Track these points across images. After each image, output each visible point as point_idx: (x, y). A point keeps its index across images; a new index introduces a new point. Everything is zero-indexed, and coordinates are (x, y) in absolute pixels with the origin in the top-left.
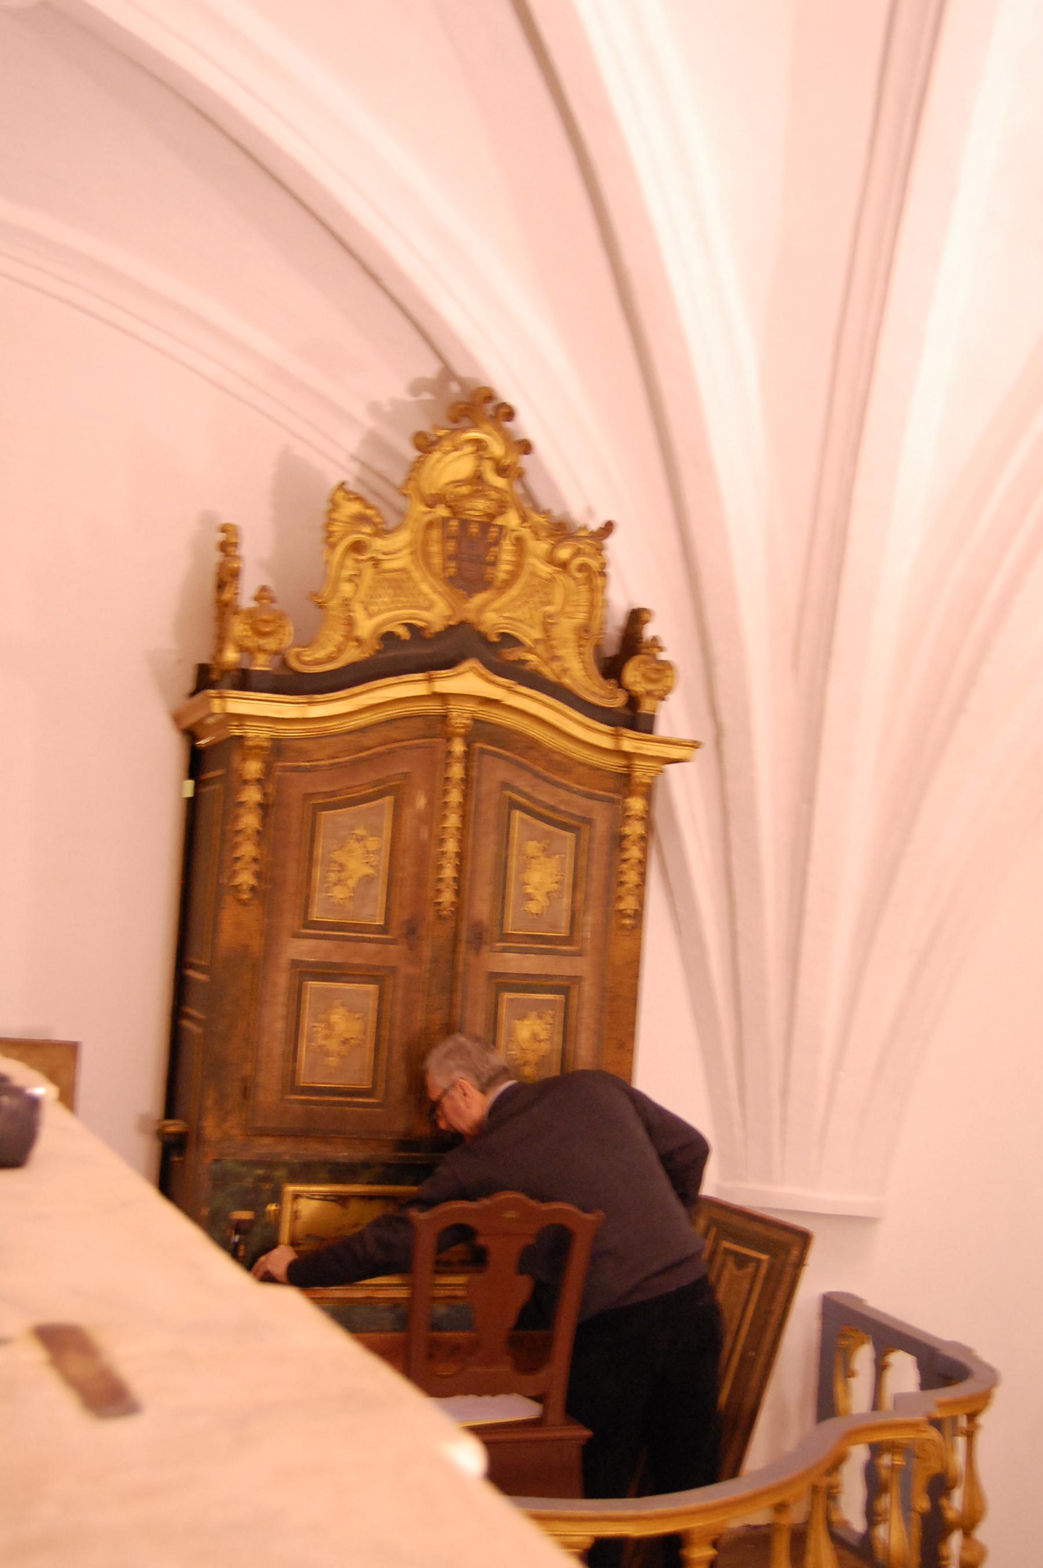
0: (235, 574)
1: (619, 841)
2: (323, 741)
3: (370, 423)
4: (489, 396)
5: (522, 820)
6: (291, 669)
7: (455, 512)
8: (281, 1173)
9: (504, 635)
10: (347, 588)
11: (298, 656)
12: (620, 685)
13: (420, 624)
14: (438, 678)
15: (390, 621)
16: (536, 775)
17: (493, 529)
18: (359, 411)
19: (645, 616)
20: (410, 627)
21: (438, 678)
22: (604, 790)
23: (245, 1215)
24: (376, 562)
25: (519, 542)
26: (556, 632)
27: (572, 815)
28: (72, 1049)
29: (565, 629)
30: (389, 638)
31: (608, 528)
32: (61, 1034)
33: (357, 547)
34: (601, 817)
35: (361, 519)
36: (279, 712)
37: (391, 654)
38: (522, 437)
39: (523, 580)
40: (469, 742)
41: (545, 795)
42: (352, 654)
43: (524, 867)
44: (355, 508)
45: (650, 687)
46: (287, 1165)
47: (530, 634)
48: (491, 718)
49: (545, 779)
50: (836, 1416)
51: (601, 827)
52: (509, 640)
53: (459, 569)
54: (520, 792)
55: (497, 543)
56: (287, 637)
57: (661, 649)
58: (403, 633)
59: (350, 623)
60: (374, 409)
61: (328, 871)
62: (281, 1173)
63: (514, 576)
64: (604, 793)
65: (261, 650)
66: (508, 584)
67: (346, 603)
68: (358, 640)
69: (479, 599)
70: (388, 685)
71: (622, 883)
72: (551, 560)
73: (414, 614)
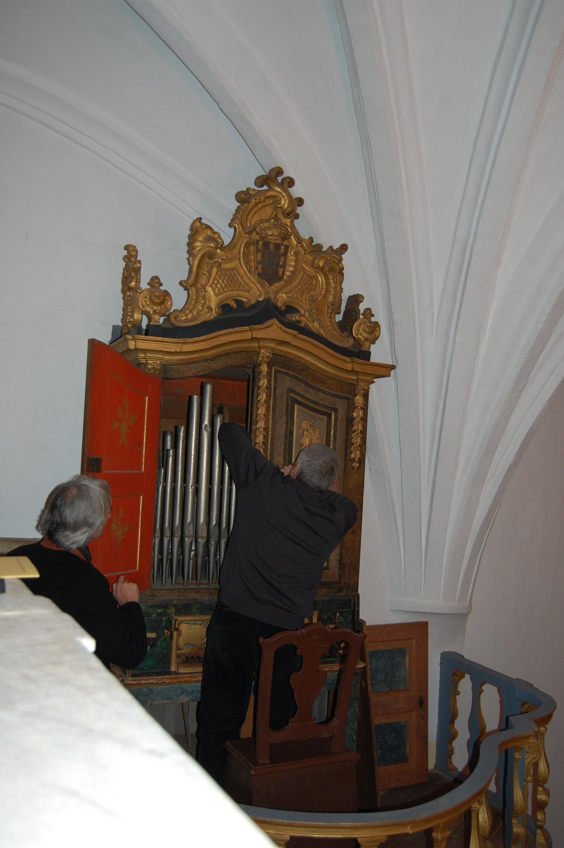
1: (350, 421)
5: (299, 409)
6: (173, 324)
11: (176, 318)
16: (306, 384)
22: (342, 392)
27: (326, 407)
31: (344, 248)
32: (174, 427)
34: (341, 406)
36: (166, 348)
40: (270, 366)
41: (312, 395)
46: (175, 606)
48: (191, 569)
51: (342, 414)
53: (263, 268)
54: (300, 395)
55: (285, 254)
57: (373, 316)
62: (172, 611)
70: (242, 331)
71: (352, 444)
72: (312, 265)
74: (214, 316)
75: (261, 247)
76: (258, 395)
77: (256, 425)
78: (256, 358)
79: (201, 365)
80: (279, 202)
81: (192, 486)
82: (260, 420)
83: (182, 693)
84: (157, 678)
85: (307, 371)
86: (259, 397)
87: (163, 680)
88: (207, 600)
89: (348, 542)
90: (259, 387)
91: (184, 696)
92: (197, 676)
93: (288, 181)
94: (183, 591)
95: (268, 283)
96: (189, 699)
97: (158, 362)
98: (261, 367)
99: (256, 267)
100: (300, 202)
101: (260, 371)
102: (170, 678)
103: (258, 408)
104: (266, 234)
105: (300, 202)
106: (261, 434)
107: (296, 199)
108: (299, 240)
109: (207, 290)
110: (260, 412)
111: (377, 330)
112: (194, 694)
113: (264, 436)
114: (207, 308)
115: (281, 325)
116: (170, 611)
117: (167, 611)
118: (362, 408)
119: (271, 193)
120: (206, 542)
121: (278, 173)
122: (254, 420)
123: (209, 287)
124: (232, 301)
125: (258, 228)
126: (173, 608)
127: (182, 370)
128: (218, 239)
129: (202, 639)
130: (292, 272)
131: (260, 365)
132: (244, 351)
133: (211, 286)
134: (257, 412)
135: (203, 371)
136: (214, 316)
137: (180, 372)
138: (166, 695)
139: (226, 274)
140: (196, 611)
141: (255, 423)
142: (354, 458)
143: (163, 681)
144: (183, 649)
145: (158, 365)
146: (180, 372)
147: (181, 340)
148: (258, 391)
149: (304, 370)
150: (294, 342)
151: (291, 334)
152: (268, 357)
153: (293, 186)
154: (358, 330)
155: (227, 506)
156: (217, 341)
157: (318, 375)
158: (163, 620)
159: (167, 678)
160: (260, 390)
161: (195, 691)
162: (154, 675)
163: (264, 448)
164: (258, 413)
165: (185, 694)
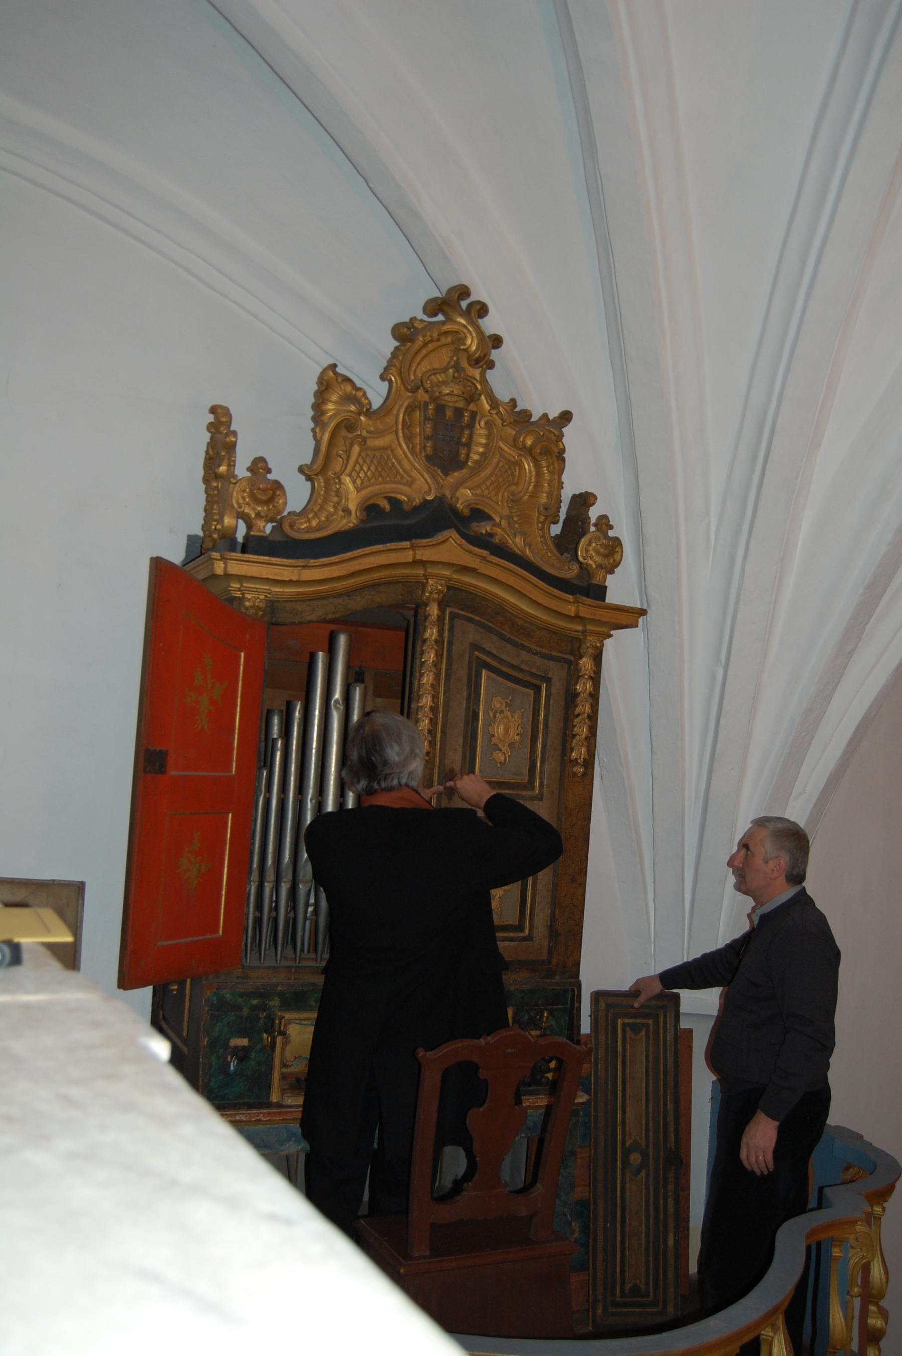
0: (231, 448)
1: (571, 698)
4: (463, 291)
5: (488, 677)
6: (286, 536)
14: (420, 546)
16: (501, 637)
19: (592, 499)
21: (420, 546)
22: (560, 652)
23: (244, 1042)
25: (489, 425)
28: (80, 887)
31: (566, 417)
37: (377, 524)
38: (492, 332)
41: (509, 654)
43: (489, 722)
46: (281, 995)
49: (510, 641)
50: (885, 1334)
51: (558, 686)
52: (478, 515)
53: (435, 448)
55: (471, 426)
57: (611, 528)
58: (385, 505)
61: (401, 785)
62: (275, 1002)
64: (559, 654)
67: (211, 461)
71: (574, 736)
72: (514, 444)
79: (331, 603)
86: (424, 656)
91: (291, 1143)
93: (478, 307)
94: (293, 970)
96: (300, 1147)
100: (497, 341)
103: (422, 675)
105: (497, 341)
109: (343, 481)
111: (618, 551)
114: (343, 511)
116: (271, 1003)
119: (450, 326)
122: (416, 695)
132: (401, 582)
133: (350, 475)
134: (420, 680)
135: (334, 613)
137: (296, 613)
140: (314, 1004)
143: (258, 1118)
145: (261, 601)
147: (300, 562)
148: (422, 646)
152: (440, 592)
158: (260, 1018)
165: (293, 1139)
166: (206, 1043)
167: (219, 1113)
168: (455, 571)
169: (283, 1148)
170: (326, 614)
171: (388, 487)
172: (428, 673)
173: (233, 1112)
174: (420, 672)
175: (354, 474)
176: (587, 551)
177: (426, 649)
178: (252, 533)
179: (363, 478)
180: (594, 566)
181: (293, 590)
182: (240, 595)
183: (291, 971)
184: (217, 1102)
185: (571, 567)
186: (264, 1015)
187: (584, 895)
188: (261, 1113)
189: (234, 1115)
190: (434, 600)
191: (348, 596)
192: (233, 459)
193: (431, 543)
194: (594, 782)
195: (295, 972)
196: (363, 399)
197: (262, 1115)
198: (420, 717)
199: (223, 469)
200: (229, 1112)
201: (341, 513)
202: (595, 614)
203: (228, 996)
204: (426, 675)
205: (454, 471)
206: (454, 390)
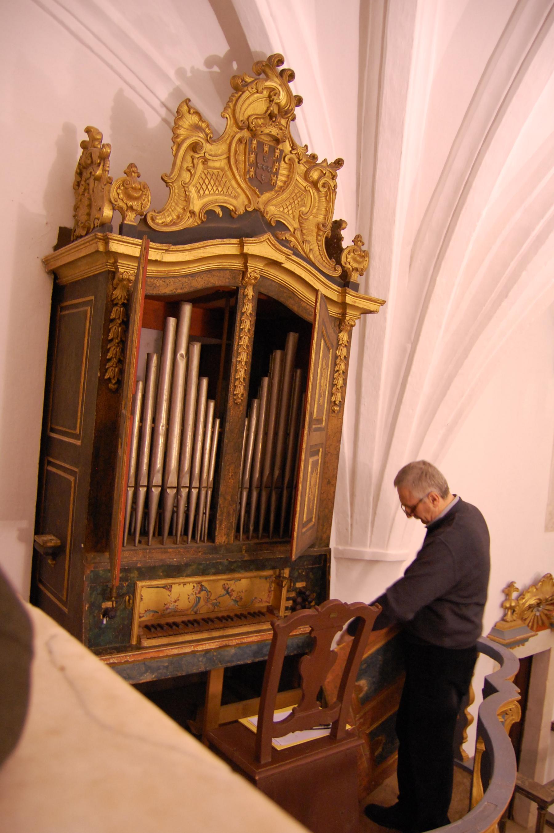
2: (168, 280)
3: (177, 83)
7: (254, 134)
8: (135, 574)
9: (278, 222)
10: (186, 176)
11: (153, 219)
12: (339, 262)
13: (231, 208)
15: (212, 202)
17: (278, 151)
18: (171, 73)
19: (343, 226)
20: (222, 207)
24: (205, 161)
26: (306, 225)
29: (311, 225)
30: (210, 213)
31: (339, 163)
33: (195, 147)
35: (197, 128)
37: (212, 225)
39: (291, 188)
42: (188, 222)
44: (195, 119)
45: (355, 265)
46: (139, 569)
47: (292, 224)
56: (148, 203)
59: (187, 199)
60: (180, 72)
62: (135, 574)
63: (286, 184)
65: (131, 208)
66: (282, 189)
68: (193, 213)
69: (266, 196)
72: (306, 177)
73: (228, 200)
74: (198, 223)
75: (255, 147)
76: (241, 322)
77: (237, 358)
78: (241, 279)
79: (180, 281)
80: (277, 94)
81: (162, 426)
82: (243, 351)
83: (146, 671)
84: (119, 655)
85: (294, 300)
86: (242, 325)
87: (126, 658)
88: (175, 561)
89: (324, 492)
90: (243, 314)
91: (148, 674)
92: (165, 650)
93: (289, 73)
94: (148, 551)
95: (259, 191)
96: (154, 676)
97: (132, 272)
98: (246, 290)
99: (247, 170)
100: (299, 101)
101: (245, 294)
102: (133, 655)
103: (240, 338)
104: (262, 132)
105: (299, 101)
106: (242, 368)
107: (296, 96)
108: (294, 147)
109: (190, 189)
110: (242, 343)
111: (366, 261)
112: (160, 671)
113: (343, 379)
114: (190, 212)
115: (276, 242)
116: (132, 575)
117: (129, 575)
118: (346, 346)
119: (270, 83)
120: (175, 494)
121: (279, 61)
122: (236, 352)
123: (193, 186)
124: (218, 207)
125: (252, 124)
126: (136, 571)
127: (158, 285)
128: (207, 129)
129: (165, 604)
130: (285, 182)
131: (245, 287)
132: (228, 269)
133: (195, 186)
134: (239, 342)
135: (181, 289)
136: (198, 223)
137: (155, 287)
138: (128, 675)
139: (208, 172)
140: (161, 574)
141: (236, 355)
142: (335, 401)
143: (126, 660)
144: (144, 616)
145: (132, 275)
146: (155, 287)
147: (164, 246)
148: (241, 317)
149: (290, 297)
150: (288, 265)
151: (285, 253)
152: (256, 278)
153: (292, 81)
154: (347, 258)
155: (145, 436)
156: (203, 252)
157: (304, 305)
158: (124, 586)
159: (130, 655)
160: (243, 317)
161: (161, 667)
162: (114, 652)
163: (244, 385)
164: (240, 344)
165: (149, 671)
166: (87, 608)
167: (98, 658)
168: (266, 265)
169: (142, 678)
170: (176, 289)
171: (221, 198)
172: (245, 336)
173: (108, 657)
174: (239, 336)
175: (198, 186)
176: (347, 258)
177: (244, 320)
178: (125, 222)
179: (204, 190)
180: (351, 269)
181: (153, 269)
182: (114, 270)
183: (146, 552)
184: (93, 648)
185: (337, 269)
186: (127, 583)
187: (334, 492)
188: (127, 656)
189: (109, 659)
190: (251, 284)
191: (192, 277)
192: (108, 165)
193: (255, 242)
194: (344, 417)
195: (149, 552)
196: (207, 129)
197: (128, 657)
198: (238, 368)
199: (99, 172)
200: (104, 657)
201: (189, 214)
202: (355, 302)
203: (101, 572)
204: (243, 338)
205: (267, 191)
206: (272, 131)
